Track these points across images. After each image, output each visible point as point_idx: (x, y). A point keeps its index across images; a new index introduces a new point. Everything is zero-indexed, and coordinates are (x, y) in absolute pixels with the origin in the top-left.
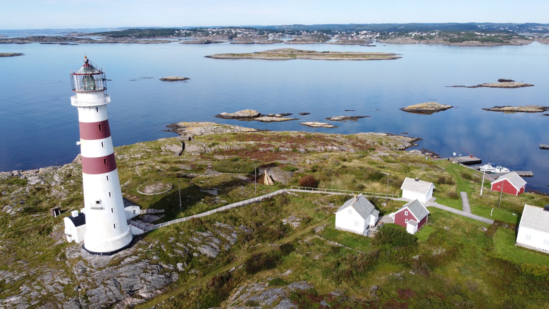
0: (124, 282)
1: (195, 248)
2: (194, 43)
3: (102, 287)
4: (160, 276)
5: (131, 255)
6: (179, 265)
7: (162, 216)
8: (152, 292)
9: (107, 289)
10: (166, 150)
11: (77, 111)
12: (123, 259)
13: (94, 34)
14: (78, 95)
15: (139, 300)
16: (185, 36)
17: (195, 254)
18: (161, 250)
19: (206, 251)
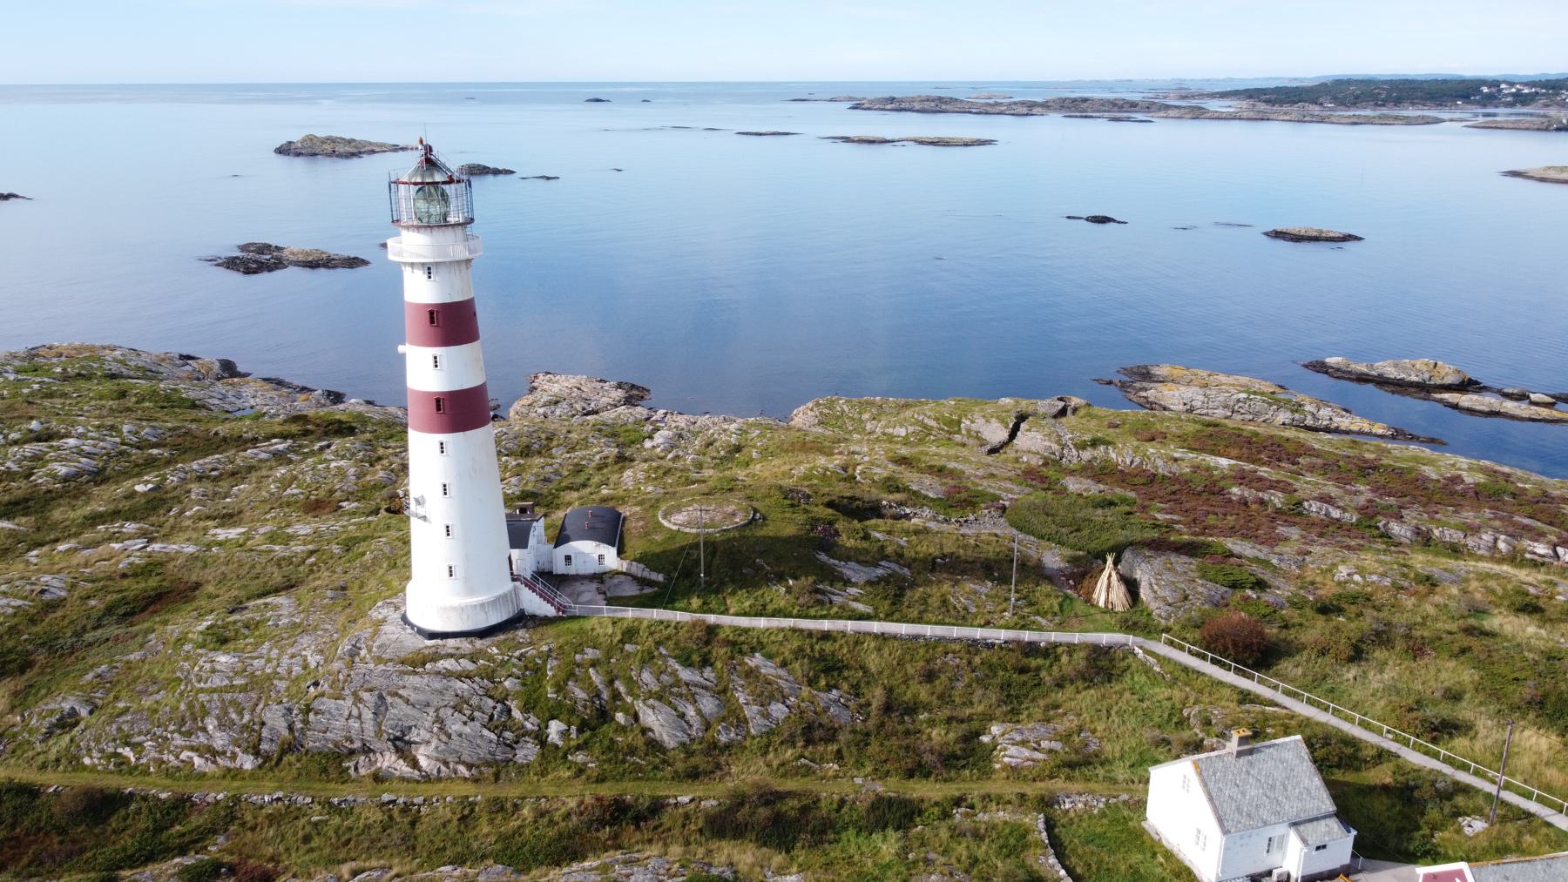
0: (398, 711)
1: (629, 699)
2: (1516, 128)
3: (349, 701)
4: (486, 732)
5: (463, 656)
6: (555, 728)
7: (647, 590)
8: (446, 763)
9: (355, 712)
10: (969, 431)
11: (401, 274)
12: (435, 658)
13: (1213, 96)
14: (404, 233)
15: (403, 768)
16: (1512, 105)
17: (620, 717)
18: (538, 671)
19: (655, 719)
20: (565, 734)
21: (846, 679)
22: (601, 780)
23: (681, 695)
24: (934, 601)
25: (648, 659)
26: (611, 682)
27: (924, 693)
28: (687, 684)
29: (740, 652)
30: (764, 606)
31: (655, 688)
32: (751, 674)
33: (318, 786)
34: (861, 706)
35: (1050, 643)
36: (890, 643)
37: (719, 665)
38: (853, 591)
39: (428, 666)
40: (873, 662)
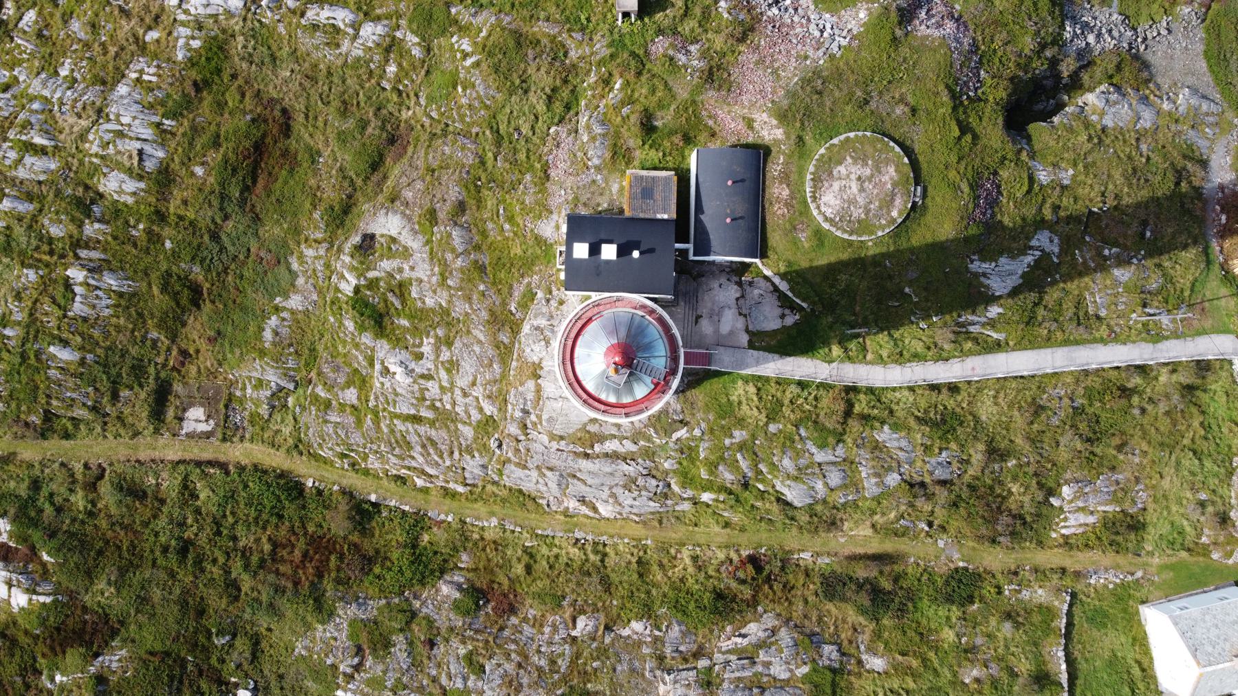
28: (820, 464)
32: (877, 447)
33: (519, 513)
36: (1008, 384)
38: (994, 311)
40: (987, 410)
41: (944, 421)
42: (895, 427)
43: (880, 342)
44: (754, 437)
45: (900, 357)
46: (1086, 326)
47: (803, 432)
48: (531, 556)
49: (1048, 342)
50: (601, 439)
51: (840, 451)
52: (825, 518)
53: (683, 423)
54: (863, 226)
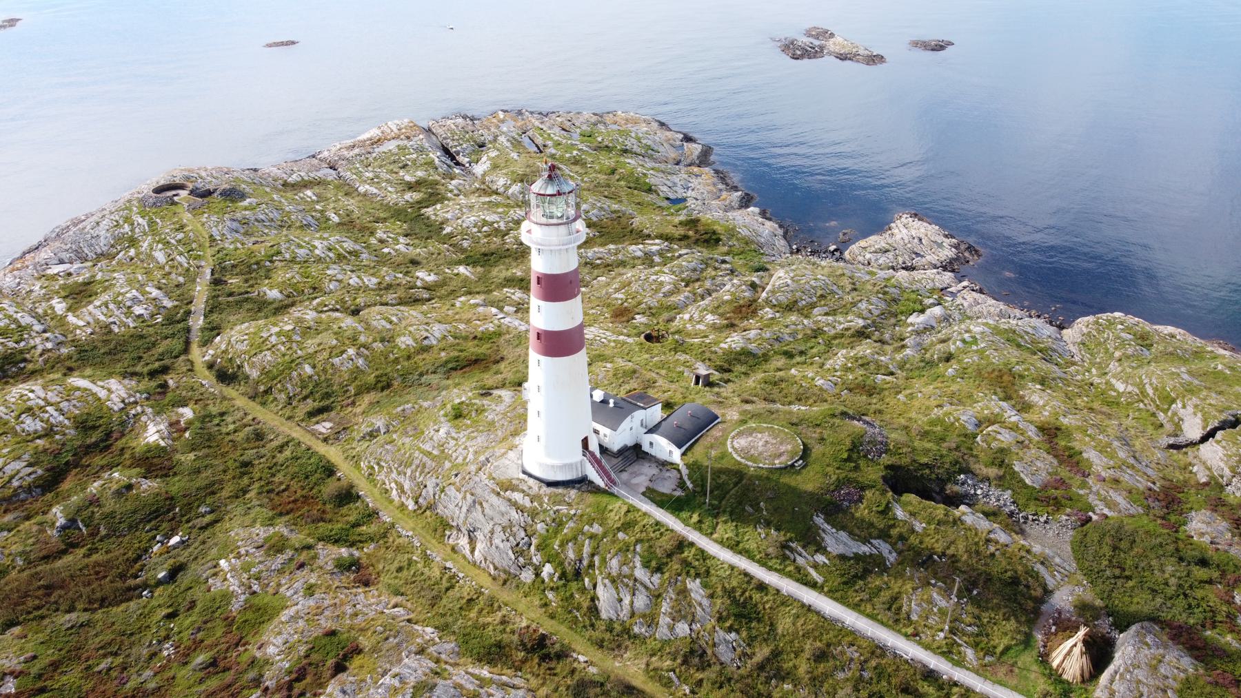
6: (548, 569)
8: (486, 559)
15: (467, 552)
18: (561, 524)
19: (605, 594)
20: (551, 576)
21: (750, 629)
22: (552, 617)
23: (627, 586)
24: (885, 596)
25: (626, 549)
26: (593, 555)
27: (803, 668)
28: (636, 580)
29: (688, 572)
30: (738, 543)
31: (614, 573)
32: (684, 592)
33: (428, 537)
34: (745, 654)
35: (950, 679)
36: (810, 615)
37: (667, 575)
38: (820, 558)
39: (508, 493)
40: (784, 624)
41: (744, 605)
42: (705, 586)
43: (726, 529)
44: (605, 535)
45: (734, 546)
46: (896, 618)
47: (638, 548)
48: (409, 565)
49: (856, 607)
50: (514, 488)
51: (656, 578)
52: (617, 637)
53: (569, 504)
54: (752, 458)
